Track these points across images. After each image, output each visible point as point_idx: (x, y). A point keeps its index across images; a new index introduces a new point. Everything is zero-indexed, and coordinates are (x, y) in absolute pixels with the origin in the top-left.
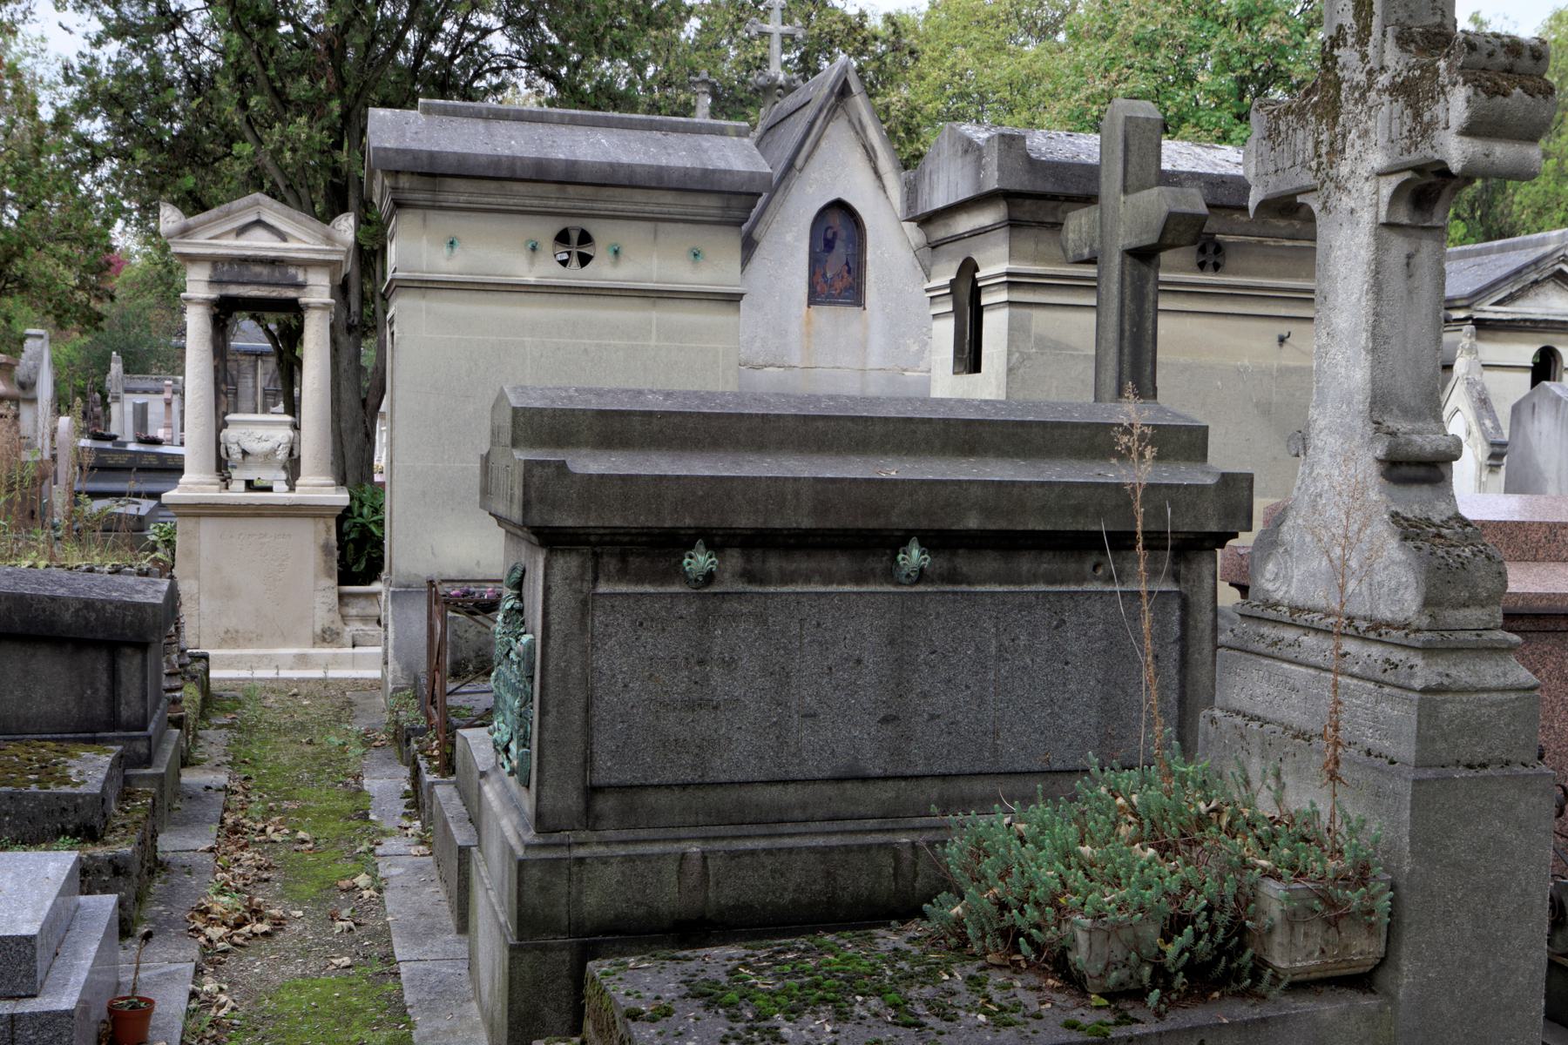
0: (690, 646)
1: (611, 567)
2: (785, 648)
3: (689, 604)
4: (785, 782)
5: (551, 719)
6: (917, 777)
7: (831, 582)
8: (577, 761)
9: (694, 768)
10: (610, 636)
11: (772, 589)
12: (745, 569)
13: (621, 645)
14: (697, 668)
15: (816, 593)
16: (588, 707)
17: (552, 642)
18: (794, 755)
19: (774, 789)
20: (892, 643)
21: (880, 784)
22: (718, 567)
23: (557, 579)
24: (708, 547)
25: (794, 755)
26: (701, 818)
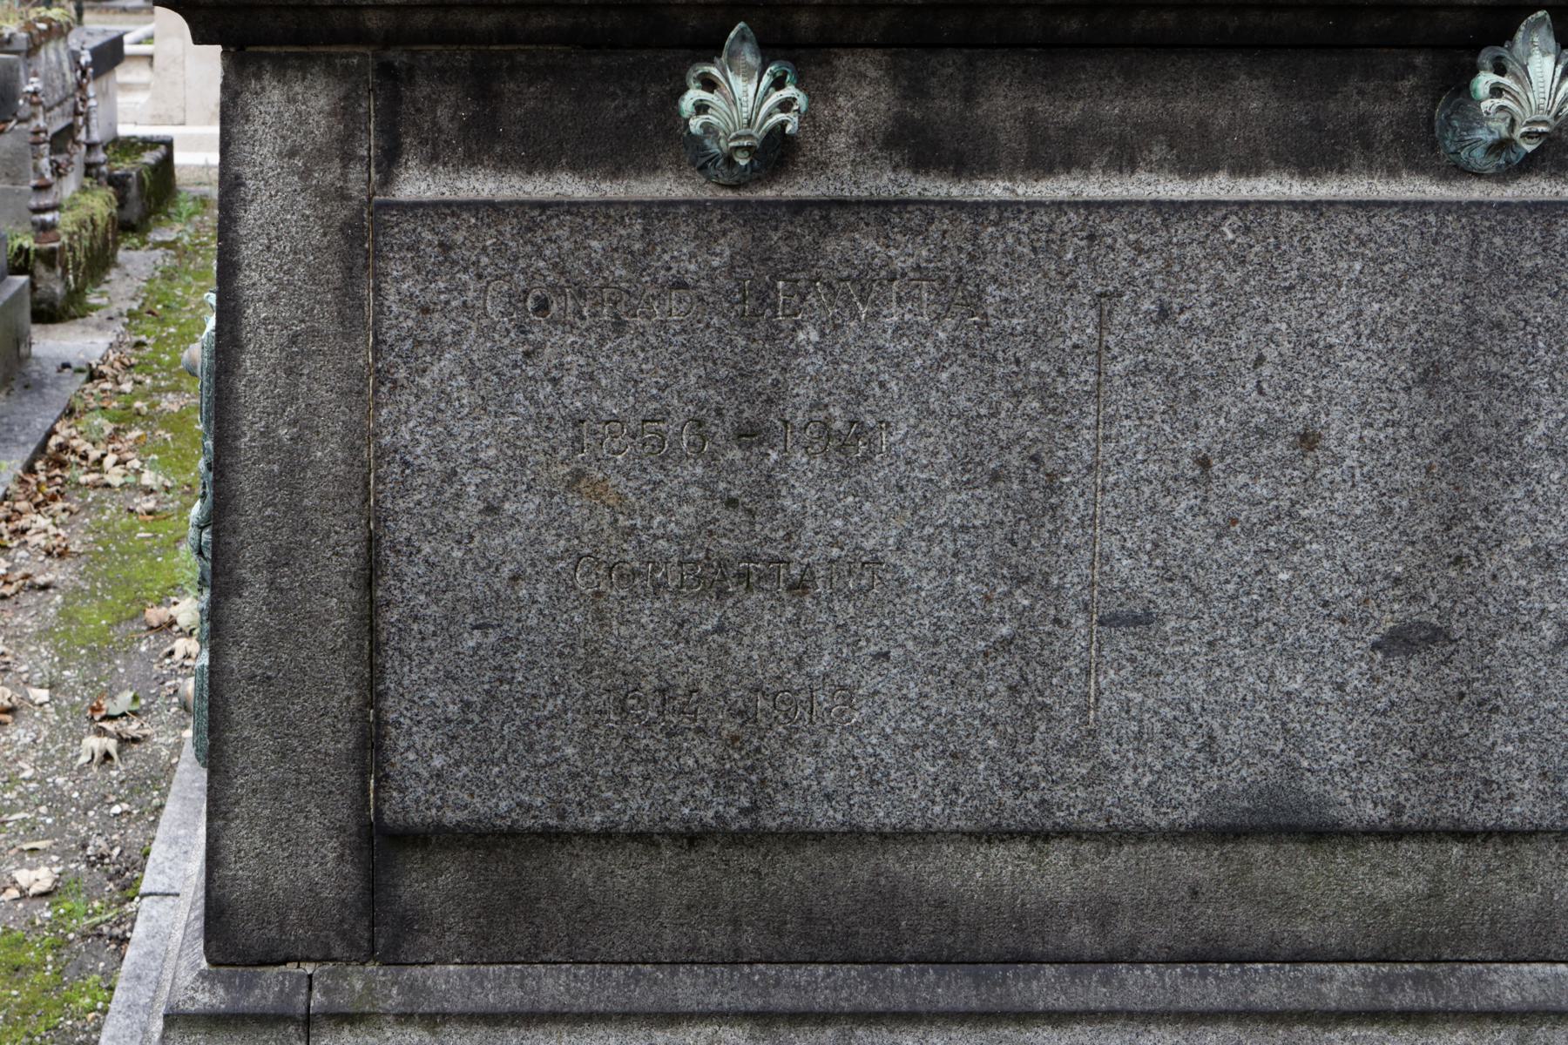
0: (709, 381)
1: (443, 113)
2: (1043, 391)
3: (708, 239)
4: (1038, 836)
5: (247, 607)
6: (1508, 835)
7: (1208, 167)
8: (338, 743)
9: (724, 780)
10: (437, 343)
11: (996, 189)
12: (901, 121)
13: (472, 372)
14: (736, 454)
15: (1157, 205)
16: (370, 572)
17: (248, 361)
18: (1072, 749)
19: (998, 852)
20: (1430, 377)
21: (1374, 850)
22: (804, 117)
23: (263, 153)
24: (769, 49)
25: (1072, 749)
26: (748, 938)
